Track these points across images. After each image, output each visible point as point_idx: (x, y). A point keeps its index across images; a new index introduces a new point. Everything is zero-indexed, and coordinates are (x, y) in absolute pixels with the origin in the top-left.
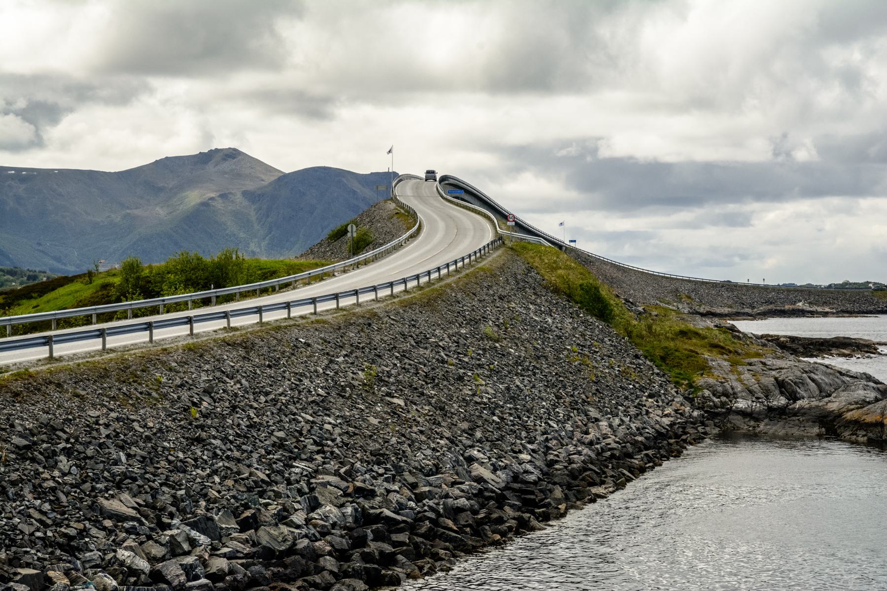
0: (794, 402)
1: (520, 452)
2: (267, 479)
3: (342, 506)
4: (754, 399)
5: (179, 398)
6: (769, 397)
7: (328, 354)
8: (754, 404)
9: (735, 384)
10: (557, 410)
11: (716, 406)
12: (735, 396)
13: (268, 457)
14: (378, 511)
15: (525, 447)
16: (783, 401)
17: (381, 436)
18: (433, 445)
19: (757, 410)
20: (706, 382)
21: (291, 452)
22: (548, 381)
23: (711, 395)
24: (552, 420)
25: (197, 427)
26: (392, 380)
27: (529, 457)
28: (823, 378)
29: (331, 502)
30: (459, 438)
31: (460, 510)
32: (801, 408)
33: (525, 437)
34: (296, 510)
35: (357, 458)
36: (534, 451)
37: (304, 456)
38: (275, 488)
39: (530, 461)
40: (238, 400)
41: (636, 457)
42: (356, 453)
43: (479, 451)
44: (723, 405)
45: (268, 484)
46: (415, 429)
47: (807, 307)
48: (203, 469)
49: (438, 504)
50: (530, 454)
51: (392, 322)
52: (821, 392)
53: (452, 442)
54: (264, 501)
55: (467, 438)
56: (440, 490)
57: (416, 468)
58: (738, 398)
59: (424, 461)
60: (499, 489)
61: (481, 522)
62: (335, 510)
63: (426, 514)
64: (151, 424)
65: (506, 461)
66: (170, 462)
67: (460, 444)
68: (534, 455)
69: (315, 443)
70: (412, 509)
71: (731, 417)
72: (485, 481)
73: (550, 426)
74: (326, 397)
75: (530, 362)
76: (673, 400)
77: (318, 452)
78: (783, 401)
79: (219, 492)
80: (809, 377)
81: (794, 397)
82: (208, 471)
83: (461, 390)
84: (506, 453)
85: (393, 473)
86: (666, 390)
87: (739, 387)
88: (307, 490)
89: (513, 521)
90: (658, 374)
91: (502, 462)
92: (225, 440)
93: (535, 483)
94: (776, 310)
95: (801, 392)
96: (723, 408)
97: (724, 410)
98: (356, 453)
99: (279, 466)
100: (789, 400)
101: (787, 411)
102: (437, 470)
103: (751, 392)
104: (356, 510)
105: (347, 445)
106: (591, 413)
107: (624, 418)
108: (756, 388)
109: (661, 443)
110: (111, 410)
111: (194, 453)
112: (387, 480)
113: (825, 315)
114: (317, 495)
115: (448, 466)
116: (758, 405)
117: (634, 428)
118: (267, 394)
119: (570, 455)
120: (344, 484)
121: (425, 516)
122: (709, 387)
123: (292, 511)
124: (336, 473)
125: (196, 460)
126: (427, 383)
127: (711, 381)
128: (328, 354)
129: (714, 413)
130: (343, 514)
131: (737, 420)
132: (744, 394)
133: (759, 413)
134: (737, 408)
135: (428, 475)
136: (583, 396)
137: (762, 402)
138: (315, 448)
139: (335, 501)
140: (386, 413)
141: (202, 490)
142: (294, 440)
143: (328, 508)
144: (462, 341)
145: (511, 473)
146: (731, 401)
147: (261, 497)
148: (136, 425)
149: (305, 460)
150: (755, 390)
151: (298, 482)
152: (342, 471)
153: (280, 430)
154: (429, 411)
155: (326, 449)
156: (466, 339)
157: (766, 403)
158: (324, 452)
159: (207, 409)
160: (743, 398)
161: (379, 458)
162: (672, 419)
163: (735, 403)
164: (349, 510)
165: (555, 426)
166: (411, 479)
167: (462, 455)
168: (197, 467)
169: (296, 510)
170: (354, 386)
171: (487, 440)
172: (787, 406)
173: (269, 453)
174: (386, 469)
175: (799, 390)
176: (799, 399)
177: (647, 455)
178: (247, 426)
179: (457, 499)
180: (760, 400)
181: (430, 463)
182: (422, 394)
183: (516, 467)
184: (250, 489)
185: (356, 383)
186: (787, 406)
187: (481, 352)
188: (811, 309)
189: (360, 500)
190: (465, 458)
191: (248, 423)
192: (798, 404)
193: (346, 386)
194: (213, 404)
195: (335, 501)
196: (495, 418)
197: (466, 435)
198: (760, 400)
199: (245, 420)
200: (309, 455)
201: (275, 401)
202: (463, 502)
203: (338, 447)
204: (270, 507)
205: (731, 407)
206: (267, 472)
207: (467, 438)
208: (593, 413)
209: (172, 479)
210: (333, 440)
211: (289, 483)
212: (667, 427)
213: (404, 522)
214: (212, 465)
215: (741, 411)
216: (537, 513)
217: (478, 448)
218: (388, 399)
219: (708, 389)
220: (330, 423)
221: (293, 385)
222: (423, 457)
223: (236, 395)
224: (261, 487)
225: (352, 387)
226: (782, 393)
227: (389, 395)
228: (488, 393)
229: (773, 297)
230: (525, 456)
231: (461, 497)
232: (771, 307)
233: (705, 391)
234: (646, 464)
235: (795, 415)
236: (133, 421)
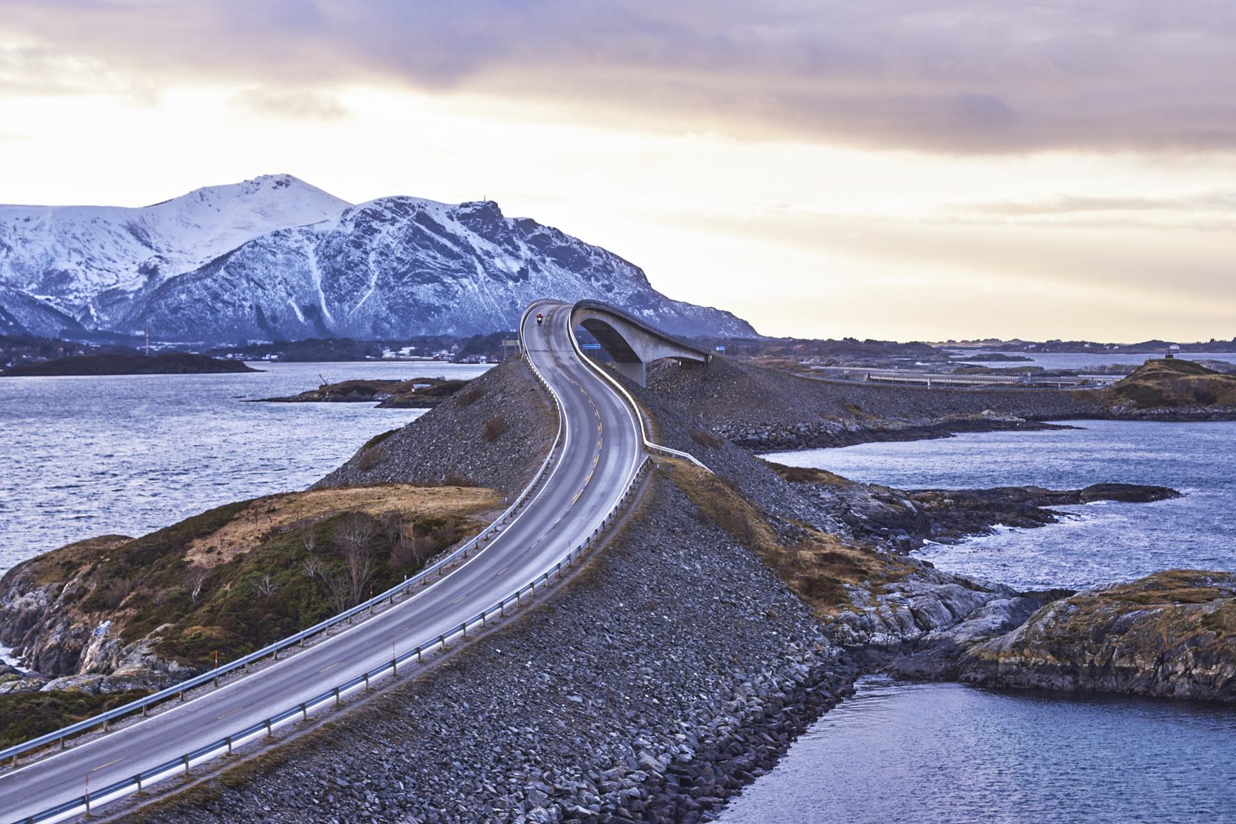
1: (677, 732)
3: (547, 807)
5: (426, 728)
9: (873, 617)
11: (855, 641)
12: (873, 628)
14: (574, 808)
15: (680, 726)
16: (916, 632)
25: (442, 753)
26: (570, 677)
27: (684, 737)
29: (540, 805)
32: (932, 640)
36: (688, 729)
37: (516, 767)
44: (861, 639)
45: (497, 795)
46: (593, 725)
47: (994, 416)
48: (453, 789)
49: (616, 796)
50: (685, 734)
57: (597, 765)
60: (661, 773)
61: (650, 806)
62: (543, 811)
64: (413, 755)
66: (431, 786)
68: (689, 733)
69: (524, 754)
70: (598, 803)
71: (868, 651)
72: (651, 768)
73: (701, 699)
77: (525, 762)
78: (916, 632)
81: (926, 628)
82: (456, 790)
86: (808, 629)
87: (877, 620)
90: (801, 609)
92: (462, 762)
93: (690, 762)
95: (934, 621)
100: (922, 630)
102: (614, 763)
103: (888, 625)
104: (557, 809)
105: (545, 751)
107: (767, 674)
108: (892, 620)
110: (386, 746)
111: (444, 776)
112: (577, 779)
120: (547, 788)
122: (849, 620)
124: (541, 779)
125: (447, 782)
126: (598, 674)
127: (851, 614)
130: (549, 814)
131: (873, 653)
135: (607, 769)
136: (730, 657)
138: (523, 758)
140: (569, 713)
144: (623, 618)
147: (493, 806)
148: (403, 757)
151: (516, 791)
152: (545, 775)
155: (531, 757)
156: (626, 613)
158: (529, 761)
160: (880, 631)
161: (570, 759)
162: (811, 664)
164: (553, 810)
165: (705, 697)
167: (631, 744)
168: (448, 787)
173: (492, 768)
174: (576, 770)
175: (932, 619)
177: (785, 712)
182: (596, 687)
183: (674, 749)
184: (485, 801)
185: (543, 687)
188: (998, 419)
189: (560, 800)
192: (934, 634)
193: (537, 691)
196: (655, 700)
201: (489, 719)
204: (501, 814)
212: (806, 675)
213: (593, 815)
218: (569, 697)
222: (602, 753)
223: (462, 718)
225: (542, 691)
226: (917, 625)
227: (570, 693)
229: (956, 402)
230: (681, 736)
231: (633, 786)
233: (845, 625)
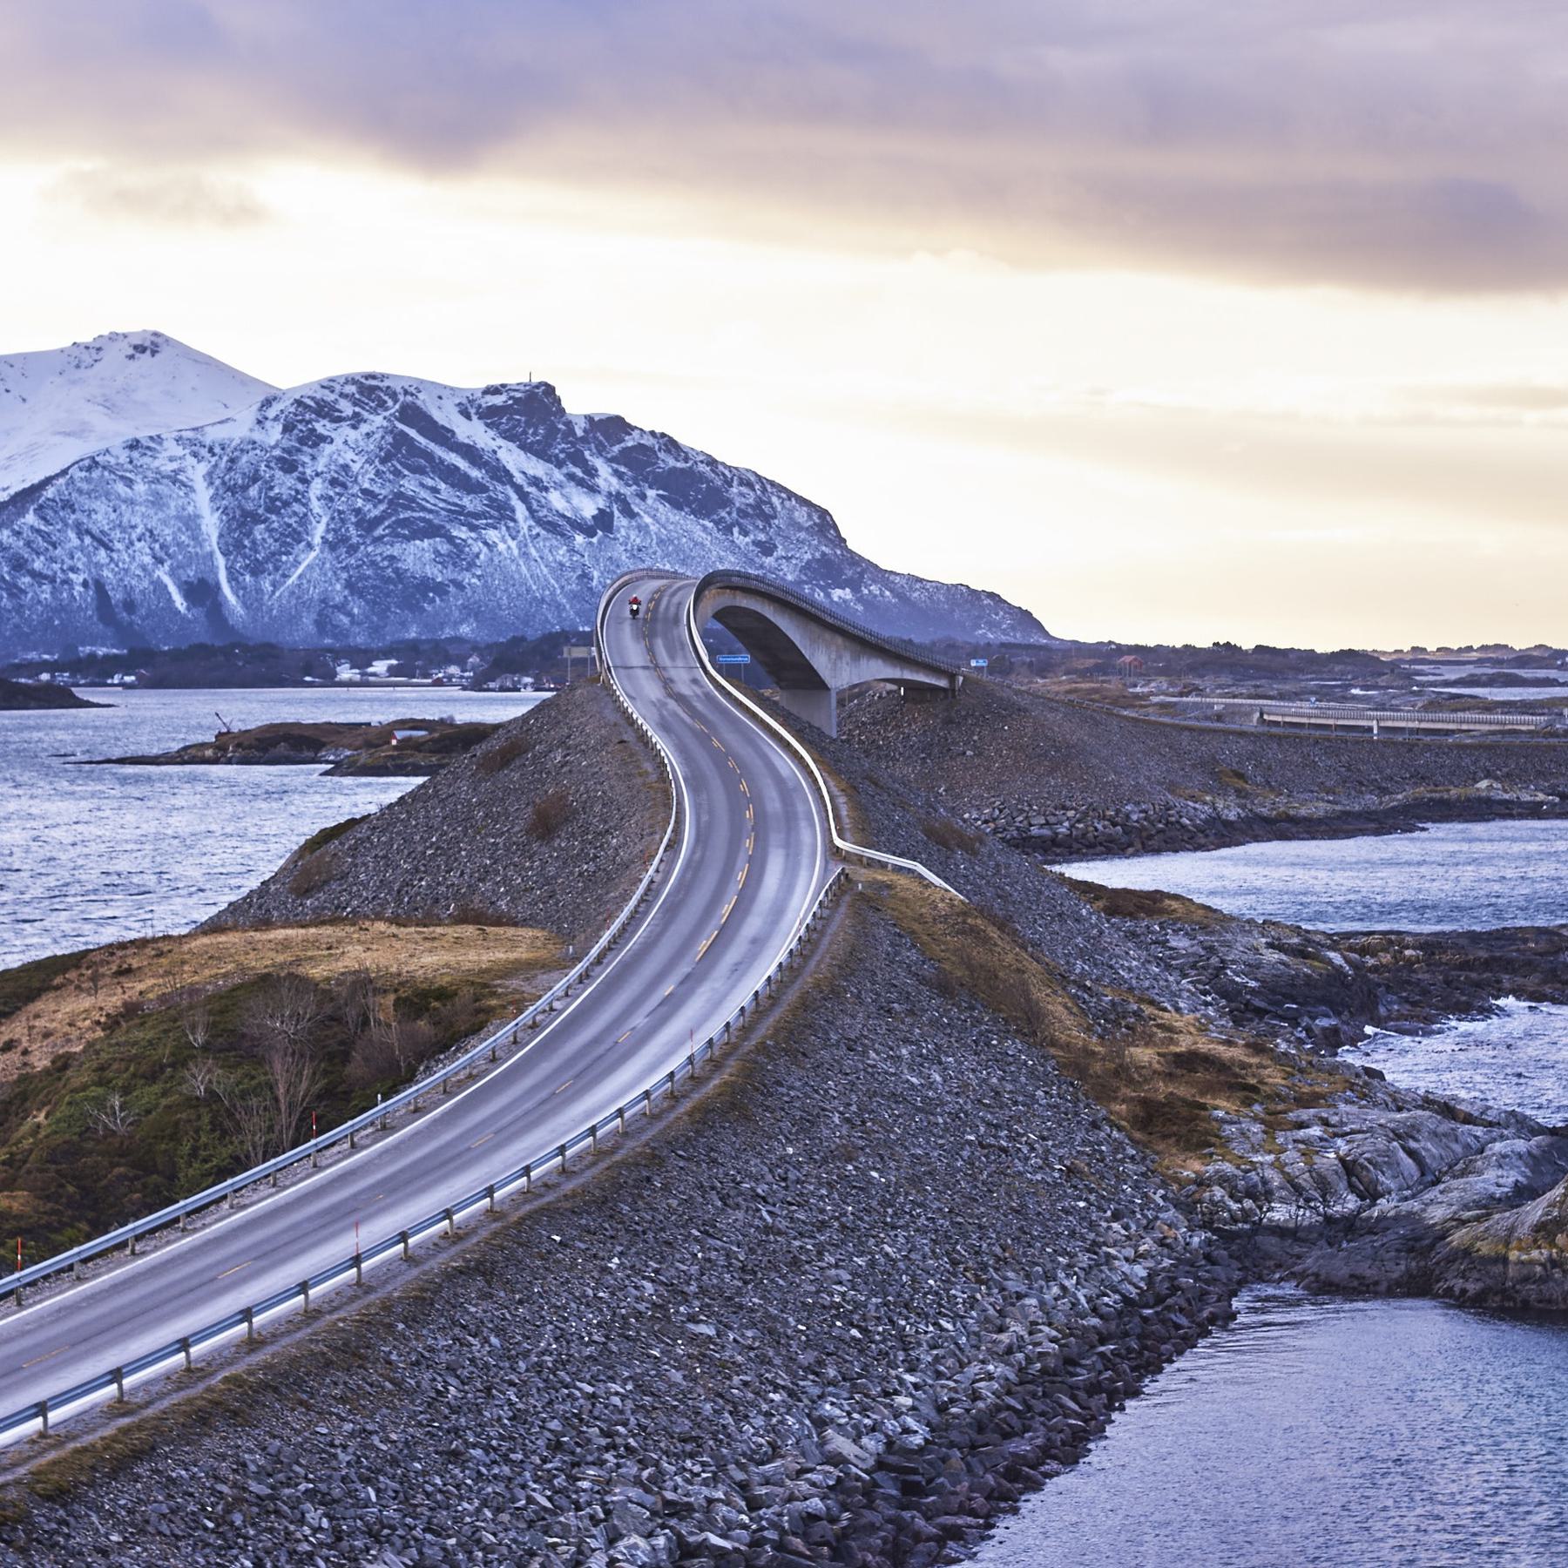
0: (1373, 1204)
1: (896, 1393)
2: (549, 1505)
3: (650, 1535)
4: (1301, 1203)
6: (1328, 1197)
7: (595, 1256)
8: (1301, 1212)
9: (1269, 1173)
10: (953, 1292)
11: (1234, 1220)
12: (1268, 1195)
13: (545, 1466)
15: (901, 1382)
16: (1352, 1203)
17: (690, 1402)
18: (765, 1407)
19: (1306, 1223)
20: (1217, 1172)
21: (573, 1453)
22: (937, 1231)
23: (1226, 1198)
24: (945, 1315)
26: (693, 1288)
27: (909, 1401)
28: (1429, 1145)
30: (801, 1383)
31: (812, 1518)
32: (1382, 1218)
33: (903, 1361)
34: (594, 1550)
35: (661, 1449)
38: (562, 1519)
39: (913, 1408)
40: (492, 1374)
41: (1084, 1362)
42: (658, 1441)
43: (832, 1404)
44: (1246, 1215)
45: (553, 1513)
46: (736, 1380)
48: (470, 1501)
49: (780, 1515)
50: (911, 1395)
51: (681, 1164)
52: (1423, 1174)
53: (791, 1394)
54: (551, 1540)
55: (813, 1381)
56: (781, 1490)
57: (744, 1454)
58: (1273, 1201)
59: (754, 1439)
61: (844, 1534)
62: (641, 1542)
63: (766, 1533)
64: (394, 1437)
65: (874, 1416)
66: (428, 1495)
67: (803, 1397)
71: (1259, 1238)
72: (846, 1461)
73: (942, 1329)
74: (604, 1344)
75: (907, 1194)
76: (1157, 1218)
77: (607, 1449)
78: (1352, 1203)
79: (495, 1535)
80: (1403, 1148)
83: (798, 1286)
84: (874, 1400)
85: (713, 1468)
86: (1146, 1195)
87: (1276, 1180)
88: (602, 1516)
89: (890, 1526)
90: (1132, 1158)
91: (868, 1417)
92: (487, 1449)
93: (921, 1450)
94: (1431, 799)
96: (1245, 1222)
97: (1247, 1226)
98: (658, 1441)
99: (560, 1481)
100: (1363, 1199)
101: (1358, 1223)
102: (775, 1452)
103: (1298, 1190)
104: (669, 1539)
106: (1009, 1284)
107: (1066, 1283)
108: (1305, 1180)
109: (1129, 1322)
112: (705, 1483)
113: (1534, 811)
114: (616, 1522)
115: (790, 1442)
116: (1308, 1214)
117: (1083, 1300)
118: (526, 1355)
119: (973, 1382)
120: (649, 1499)
121: (764, 1537)
122: (1223, 1180)
123: (588, 1552)
124: (638, 1482)
126: (746, 1283)
127: (1228, 1168)
128: (595, 1256)
129: (1230, 1231)
130: (654, 1548)
131: (1270, 1243)
132: (1284, 1193)
133: (1311, 1227)
134: (1270, 1220)
135: (763, 1464)
137: (1315, 1208)
138: (603, 1442)
139: (642, 1529)
140: (690, 1356)
141: (474, 1533)
142: (574, 1433)
143: (632, 1541)
145: (882, 1437)
146: (1261, 1208)
147: (546, 1533)
149: (594, 1464)
150: (1304, 1184)
151: (589, 1504)
152: (645, 1474)
153: (553, 1418)
154: (754, 1338)
155: (618, 1440)
156: (798, 1167)
157: (1321, 1209)
158: (614, 1447)
159: (455, 1398)
160: (1283, 1200)
163: (1268, 1210)
164: (661, 1541)
165: (949, 1326)
166: (740, 1476)
167: (809, 1416)
169: (594, 1550)
170: (640, 1313)
171: (844, 1379)
172: (1359, 1213)
173: (544, 1461)
174: (703, 1464)
175: (1381, 1178)
176: (1382, 1196)
178: (509, 1419)
179: (806, 1499)
180: (1312, 1204)
181: (763, 1441)
182: (741, 1307)
183: (891, 1425)
185: (642, 1307)
186: (1359, 1213)
187: (824, 1192)
188: (1507, 796)
189: (673, 1522)
190: (812, 1421)
191: (511, 1414)
194: (461, 1387)
195: (642, 1529)
197: (811, 1377)
198: (1312, 1204)
199: (506, 1408)
200: (596, 1454)
201: (539, 1368)
202: (816, 1504)
203: (634, 1436)
205: (1261, 1219)
206: (549, 1493)
207: (813, 1381)
208: (1015, 1283)
209: (435, 1521)
210: (625, 1425)
211: (578, 1508)
212: (1142, 1284)
214: (479, 1492)
215: (1278, 1227)
216: (924, 1504)
217: (831, 1399)
218: (691, 1326)
219: (1220, 1185)
220: (617, 1394)
221: (558, 1331)
222: (752, 1432)
224: (544, 1519)
225: (639, 1315)
226: (1352, 1188)
228: (840, 1283)
230: (904, 1401)
231: (812, 1496)
232: (1422, 791)
233: (1216, 1188)
234: (1100, 1373)
235: (1371, 1232)
236: (371, 1433)
